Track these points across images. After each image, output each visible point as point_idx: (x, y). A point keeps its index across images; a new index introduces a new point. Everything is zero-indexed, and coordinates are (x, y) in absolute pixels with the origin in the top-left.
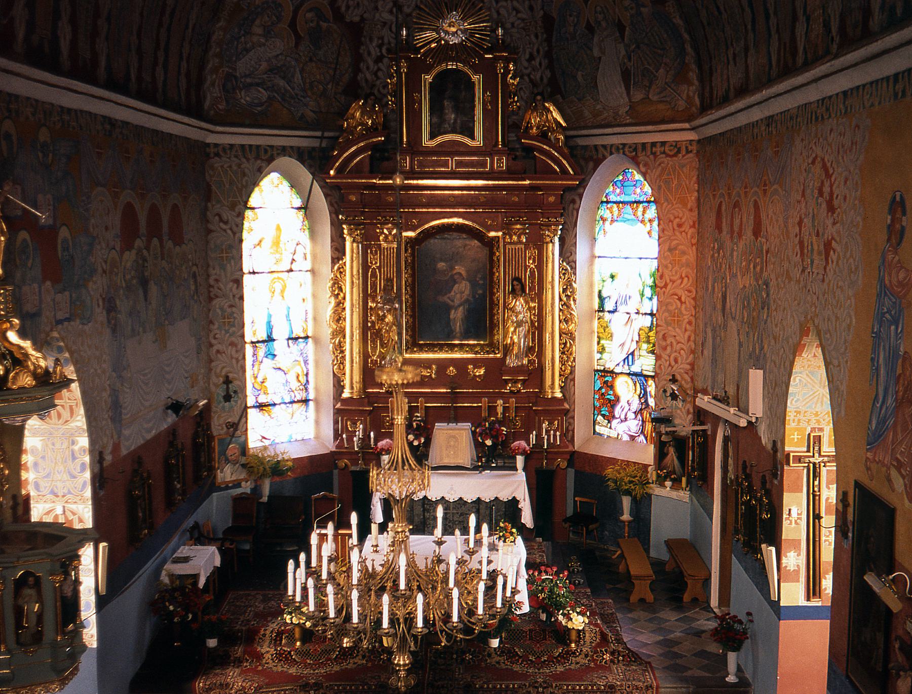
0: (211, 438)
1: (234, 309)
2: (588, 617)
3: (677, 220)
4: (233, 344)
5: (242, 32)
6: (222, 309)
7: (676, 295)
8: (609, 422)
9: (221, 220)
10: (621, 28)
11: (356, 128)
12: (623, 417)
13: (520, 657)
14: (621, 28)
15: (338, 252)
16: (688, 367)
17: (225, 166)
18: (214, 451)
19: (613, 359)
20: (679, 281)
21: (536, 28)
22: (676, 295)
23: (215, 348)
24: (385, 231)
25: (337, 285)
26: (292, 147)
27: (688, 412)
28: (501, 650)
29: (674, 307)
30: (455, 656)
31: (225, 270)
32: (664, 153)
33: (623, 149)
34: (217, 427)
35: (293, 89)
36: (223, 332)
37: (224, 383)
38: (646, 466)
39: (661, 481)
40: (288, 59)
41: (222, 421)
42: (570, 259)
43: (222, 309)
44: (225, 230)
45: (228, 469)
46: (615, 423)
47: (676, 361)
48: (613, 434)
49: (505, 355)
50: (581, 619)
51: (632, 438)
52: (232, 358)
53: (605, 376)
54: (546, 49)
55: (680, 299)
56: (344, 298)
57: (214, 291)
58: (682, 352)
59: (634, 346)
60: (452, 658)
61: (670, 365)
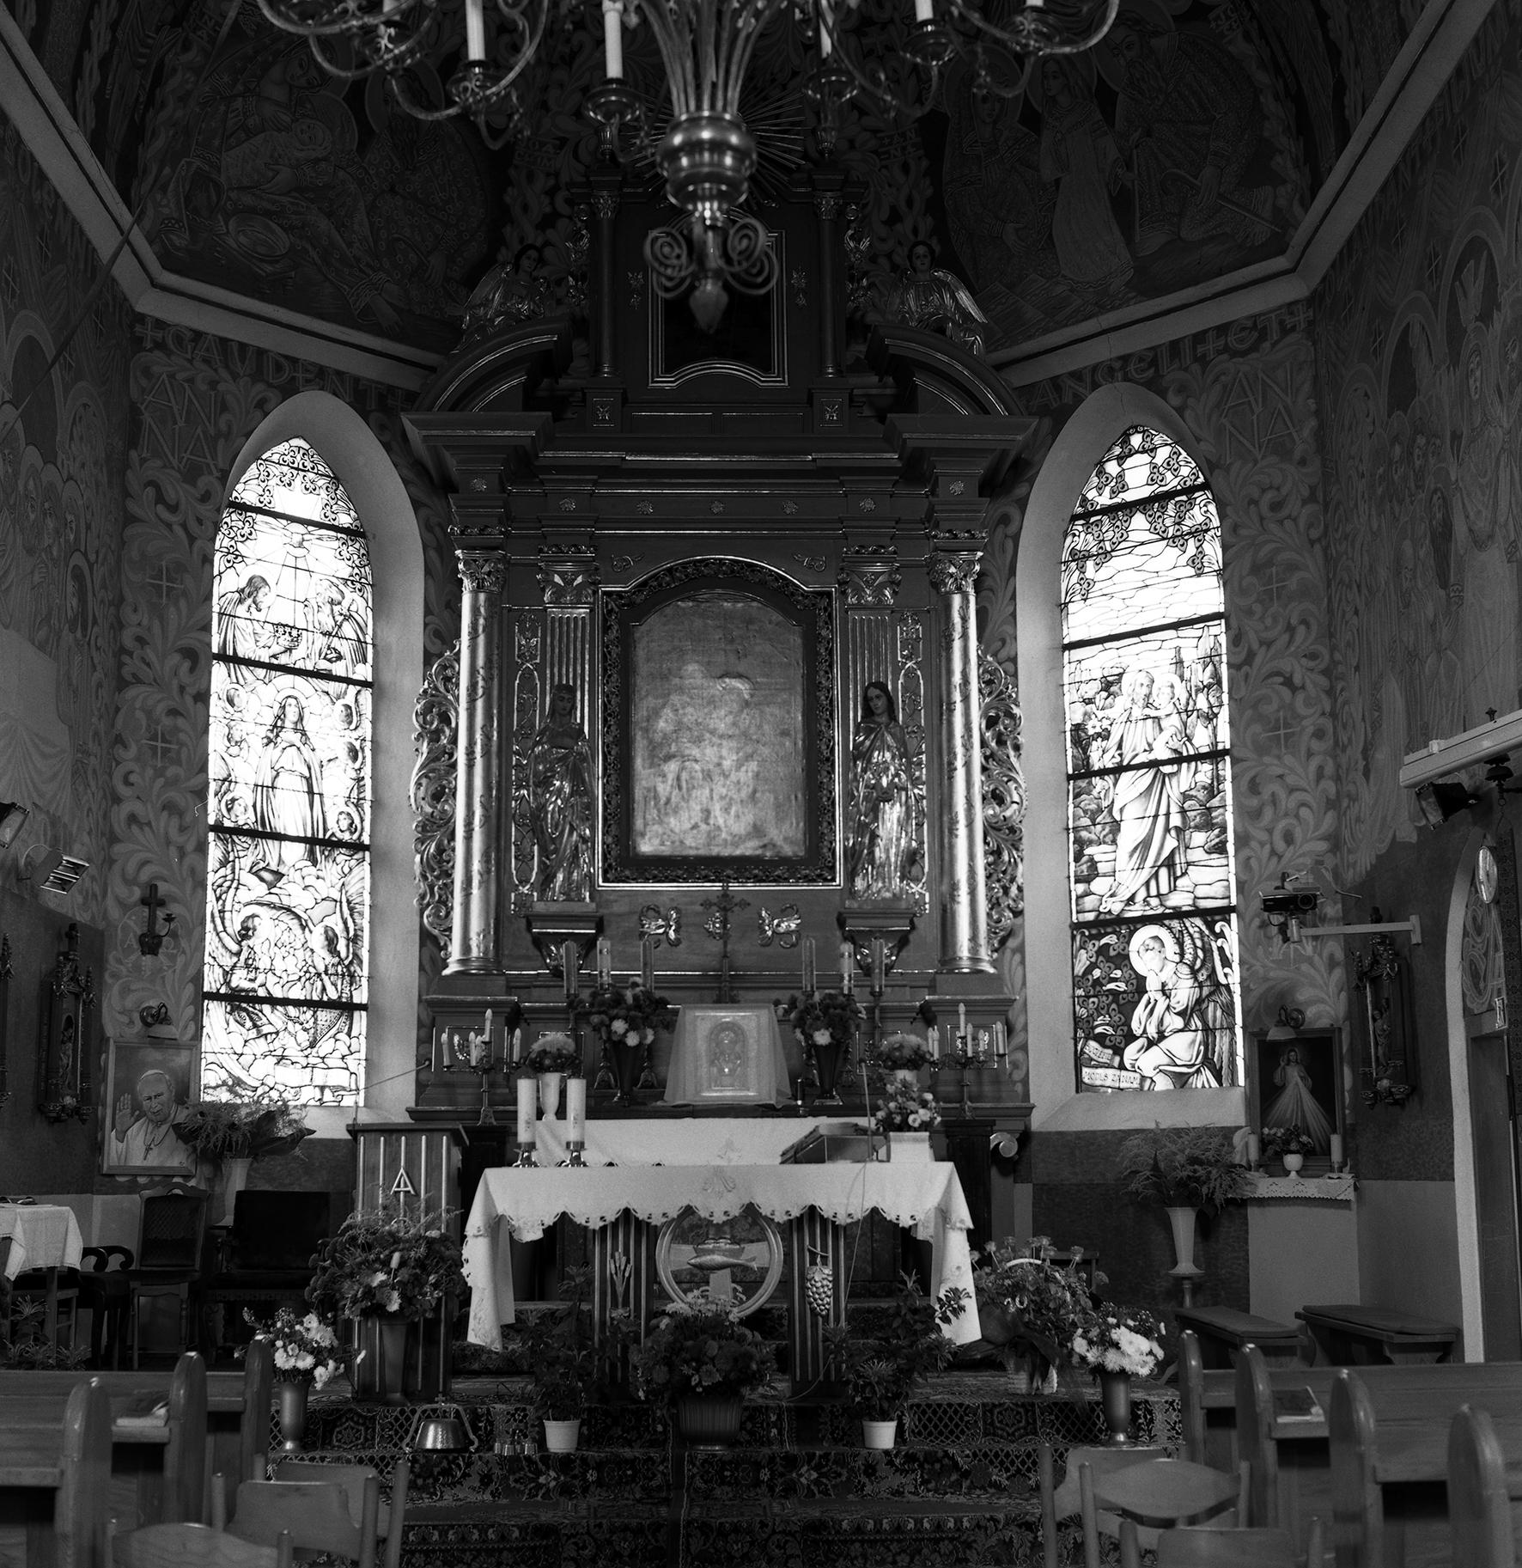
0: (96, 1041)
1: (180, 721)
2: (1161, 1341)
3: (1269, 495)
4: (170, 807)
5: (240, 87)
6: (149, 713)
7: (1278, 674)
8: (1119, 1051)
9: (160, 499)
10: (1105, 98)
11: (492, 320)
12: (1152, 1031)
13: (965, 1474)
14: (1105, 98)
15: (441, 633)
16: (1323, 846)
17: (180, 376)
18: (105, 1079)
19: (1121, 880)
20: (1286, 637)
21: (904, 148)
22: (1278, 674)
23: (126, 809)
24: (557, 579)
25: (436, 712)
26: (339, 373)
27: (1332, 964)
28: (903, 1458)
29: (1275, 706)
30: (765, 1475)
31: (162, 620)
32: (1226, 349)
33: (1122, 368)
34: (117, 1014)
35: (350, 245)
36: (150, 772)
37: (144, 902)
38: (1227, 1133)
39: (1271, 1161)
40: (341, 174)
41: (129, 1002)
42: (1003, 654)
43: (149, 713)
44: (169, 526)
45: (138, 1135)
46: (1131, 1052)
47: (1289, 838)
48: (1128, 1080)
49: (851, 876)
50: (1144, 1344)
51: (1181, 1080)
52: (168, 843)
53: (1099, 936)
54: (929, 192)
55: (1288, 682)
56: (454, 740)
57: (131, 666)
58: (1304, 812)
59: (1171, 843)
60: (757, 1483)
61: (1273, 852)
